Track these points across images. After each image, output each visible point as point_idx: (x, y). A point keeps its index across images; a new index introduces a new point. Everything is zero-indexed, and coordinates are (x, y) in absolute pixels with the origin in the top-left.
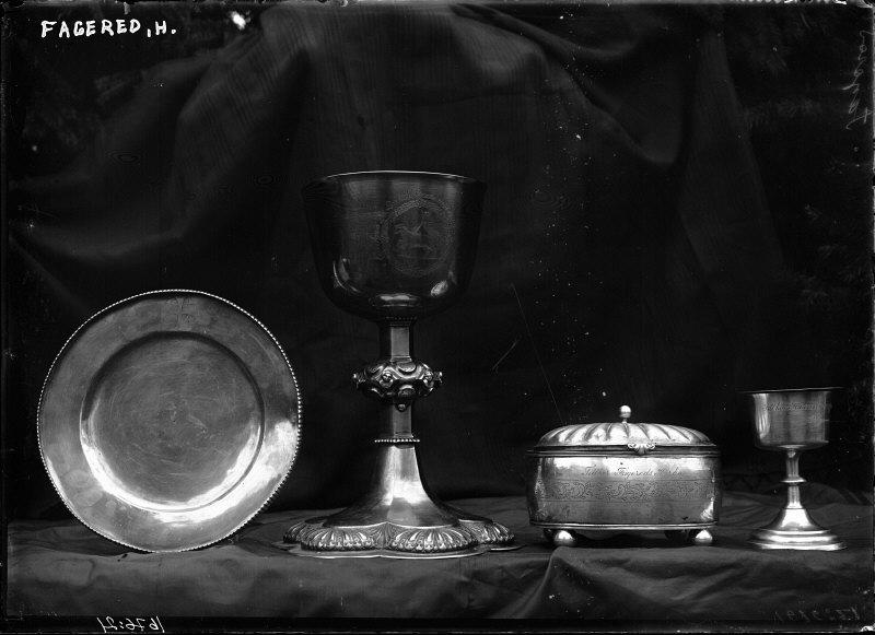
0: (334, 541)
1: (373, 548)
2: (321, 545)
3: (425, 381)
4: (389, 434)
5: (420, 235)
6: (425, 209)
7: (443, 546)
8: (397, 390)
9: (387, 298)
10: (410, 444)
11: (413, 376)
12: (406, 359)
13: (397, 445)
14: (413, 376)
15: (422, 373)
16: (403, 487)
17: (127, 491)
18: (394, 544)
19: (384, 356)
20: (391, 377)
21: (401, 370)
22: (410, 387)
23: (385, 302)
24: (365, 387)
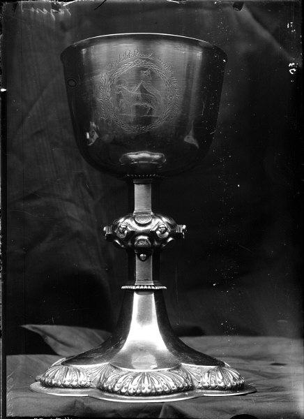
0: (69, 379)
1: (88, 387)
2: (53, 382)
3: (158, 232)
4: (132, 280)
5: (140, 93)
6: (145, 69)
7: (146, 390)
8: (133, 241)
9: (133, 156)
10: (150, 291)
11: (148, 227)
12: (146, 213)
13: (138, 291)
14: (148, 227)
15: (159, 224)
16: (144, 331)
17: (139, 301)
18: (105, 386)
19: (128, 211)
20: (126, 229)
21: (145, 221)
22: (146, 238)
23: (131, 160)
24: (112, 237)
